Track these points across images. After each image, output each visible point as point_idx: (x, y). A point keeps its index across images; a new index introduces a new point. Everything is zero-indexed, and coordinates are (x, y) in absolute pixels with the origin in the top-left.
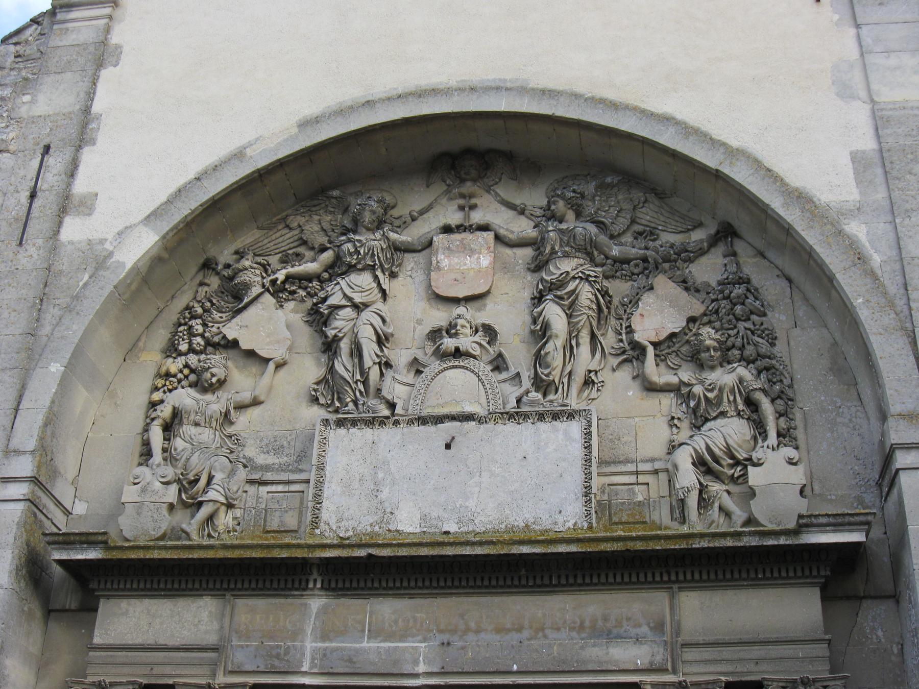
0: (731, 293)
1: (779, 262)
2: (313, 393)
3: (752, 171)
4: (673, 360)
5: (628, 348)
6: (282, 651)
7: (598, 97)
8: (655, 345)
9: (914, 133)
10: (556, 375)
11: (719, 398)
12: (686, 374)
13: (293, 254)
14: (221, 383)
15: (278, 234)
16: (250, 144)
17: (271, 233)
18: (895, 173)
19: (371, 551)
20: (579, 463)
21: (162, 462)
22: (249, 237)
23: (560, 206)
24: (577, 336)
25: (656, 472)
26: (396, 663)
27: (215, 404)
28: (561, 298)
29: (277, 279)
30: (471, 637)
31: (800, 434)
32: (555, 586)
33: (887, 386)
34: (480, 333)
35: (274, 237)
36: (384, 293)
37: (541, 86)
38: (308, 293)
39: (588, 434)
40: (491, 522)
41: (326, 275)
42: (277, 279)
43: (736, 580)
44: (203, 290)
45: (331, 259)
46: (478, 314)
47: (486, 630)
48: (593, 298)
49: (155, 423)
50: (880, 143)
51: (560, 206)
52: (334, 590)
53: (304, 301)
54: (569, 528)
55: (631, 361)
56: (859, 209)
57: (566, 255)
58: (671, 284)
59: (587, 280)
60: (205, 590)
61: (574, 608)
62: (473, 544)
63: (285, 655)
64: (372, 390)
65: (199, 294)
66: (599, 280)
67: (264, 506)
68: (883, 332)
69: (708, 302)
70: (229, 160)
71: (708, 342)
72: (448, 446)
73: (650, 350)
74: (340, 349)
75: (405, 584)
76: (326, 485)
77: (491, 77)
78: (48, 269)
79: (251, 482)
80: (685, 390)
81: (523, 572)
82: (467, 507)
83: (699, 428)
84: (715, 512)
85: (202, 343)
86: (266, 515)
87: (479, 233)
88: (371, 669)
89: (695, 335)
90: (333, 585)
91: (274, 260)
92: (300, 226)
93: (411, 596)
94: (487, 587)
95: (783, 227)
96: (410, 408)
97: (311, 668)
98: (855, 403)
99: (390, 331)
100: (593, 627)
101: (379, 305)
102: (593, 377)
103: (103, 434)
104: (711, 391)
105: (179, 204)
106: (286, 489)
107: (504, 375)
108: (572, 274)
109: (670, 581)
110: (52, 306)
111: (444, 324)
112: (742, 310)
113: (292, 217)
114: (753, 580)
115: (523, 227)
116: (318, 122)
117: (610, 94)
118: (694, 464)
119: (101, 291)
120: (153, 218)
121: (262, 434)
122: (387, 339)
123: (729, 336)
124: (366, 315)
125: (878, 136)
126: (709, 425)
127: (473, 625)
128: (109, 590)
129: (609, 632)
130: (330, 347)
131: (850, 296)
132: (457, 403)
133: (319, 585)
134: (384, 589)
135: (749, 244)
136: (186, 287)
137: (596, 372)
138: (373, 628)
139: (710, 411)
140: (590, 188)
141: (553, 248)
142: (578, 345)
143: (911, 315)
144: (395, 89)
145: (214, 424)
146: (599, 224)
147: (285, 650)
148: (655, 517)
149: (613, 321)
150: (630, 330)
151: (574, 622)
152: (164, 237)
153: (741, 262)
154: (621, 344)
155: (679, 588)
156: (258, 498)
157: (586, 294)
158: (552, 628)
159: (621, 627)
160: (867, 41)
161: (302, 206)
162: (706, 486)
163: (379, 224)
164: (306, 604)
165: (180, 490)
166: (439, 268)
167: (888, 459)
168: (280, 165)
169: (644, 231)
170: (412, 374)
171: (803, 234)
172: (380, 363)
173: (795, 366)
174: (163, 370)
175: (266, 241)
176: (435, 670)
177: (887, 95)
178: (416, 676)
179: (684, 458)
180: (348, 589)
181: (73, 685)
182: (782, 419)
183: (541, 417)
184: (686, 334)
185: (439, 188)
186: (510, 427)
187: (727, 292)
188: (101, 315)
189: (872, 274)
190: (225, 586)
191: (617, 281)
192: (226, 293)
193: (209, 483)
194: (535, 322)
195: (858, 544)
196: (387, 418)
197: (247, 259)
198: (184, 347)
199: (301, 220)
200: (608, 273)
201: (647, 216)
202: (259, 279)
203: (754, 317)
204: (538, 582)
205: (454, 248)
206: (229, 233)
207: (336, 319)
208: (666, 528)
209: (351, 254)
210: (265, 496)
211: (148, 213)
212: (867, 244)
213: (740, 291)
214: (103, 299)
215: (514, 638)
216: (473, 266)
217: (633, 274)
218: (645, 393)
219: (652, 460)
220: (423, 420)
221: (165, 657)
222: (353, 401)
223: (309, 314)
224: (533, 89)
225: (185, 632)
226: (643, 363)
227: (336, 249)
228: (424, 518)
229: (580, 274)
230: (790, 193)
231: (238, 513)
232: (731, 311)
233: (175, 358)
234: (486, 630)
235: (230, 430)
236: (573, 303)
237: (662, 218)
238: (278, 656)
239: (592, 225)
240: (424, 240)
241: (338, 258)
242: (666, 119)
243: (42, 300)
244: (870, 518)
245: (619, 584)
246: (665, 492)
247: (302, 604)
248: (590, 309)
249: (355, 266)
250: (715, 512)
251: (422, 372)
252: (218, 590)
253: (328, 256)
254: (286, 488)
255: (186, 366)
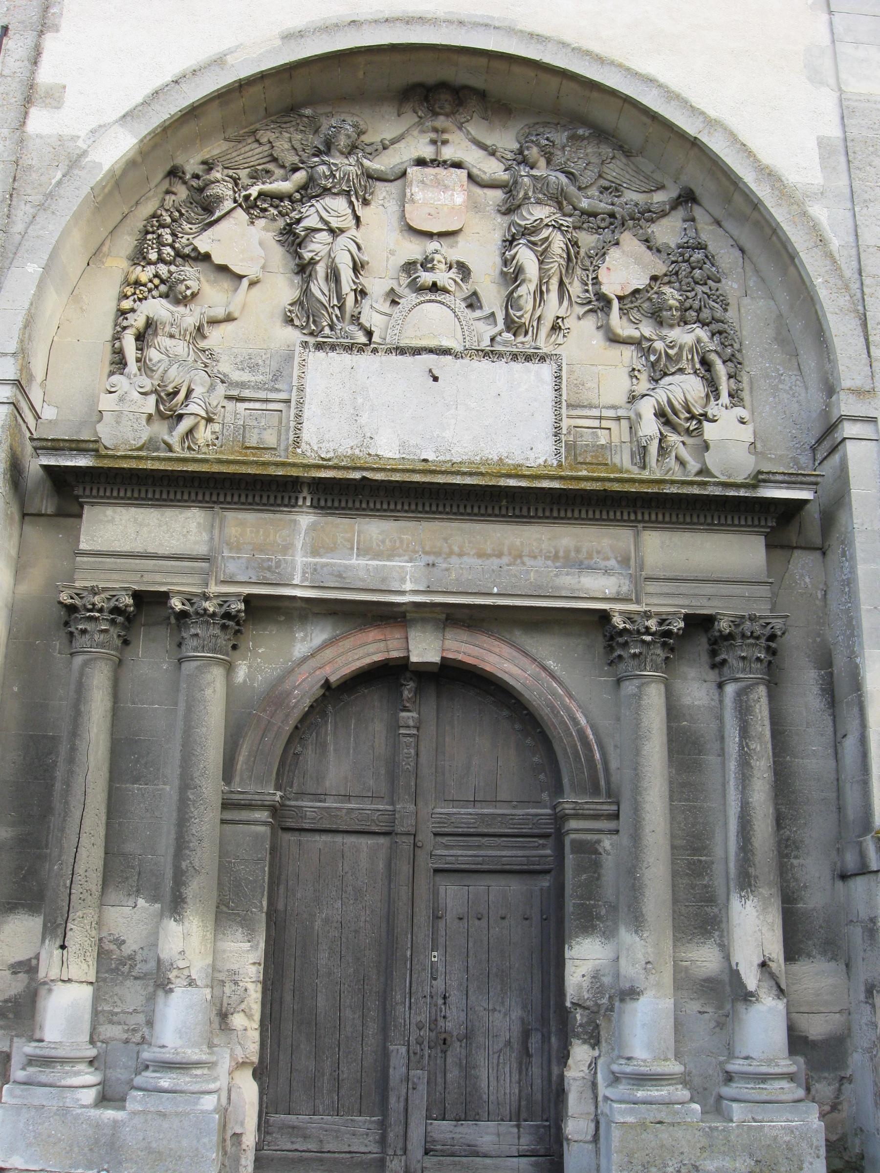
0: (691, 256)
1: (736, 233)
2: (289, 314)
3: (728, 143)
4: (635, 315)
5: (594, 299)
6: (273, 564)
7: (584, 49)
8: (620, 298)
9: (876, 126)
10: (526, 319)
11: (679, 355)
12: (647, 329)
13: (262, 170)
14: (194, 295)
15: (247, 148)
16: (230, 52)
17: (240, 146)
18: (856, 163)
19: (366, 474)
20: (550, 404)
21: (138, 373)
22: (214, 149)
23: (533, 152)
24: (547, 282)
25: (618, 419)
26: (384, 580)
27: (189, 317)
28: (534, 244)
29: (250, 195)
30: (454, 560)
31: (746, 395)
32: (533, 517)
33: (840, 362)
34: (454, 270)
35: (243, 151)
36: (357, 219)
37: (529, 30)
38: (280, 212)
39: (558, 377)
40: (467, 454)
41: (297, 196)
42: (250, 195)
43: (694, 524)
44: (170, 199)
45: (304, 180)
46: (450, 250)
47: (469, 554)
48: (564, 247)
49: (127, 331)
50: (845, 132)
51: (533, 152)
52: (322, 508)
53: (276, 220)
54: (540, 465)
55: (595, 312)
56: (822, 193)
57: (539, 202)
58: (636, 242)
59: (559, 228)
60: (193, 501)
61: (550, 539)
62: (464, 474)
63: (277, 567)
64: (348, 316)
65: (167, 202)
66: (570, 230)
67: (242, 423)
68: (838, 312)
69: (668, 262)
70: (209, 65)
71: (672, 302)
72: (436, 379)
73: (616, 304)
74: (316, 272)
75: (392, 506)
76: (306, 406)
77: (479, 13)
78: (17, 163)
79: (229, 398)
80: (645, 345)
81: (504, 503)
82: (444, 438)
83: (656, 381)
84: (671, 461)
85: (172, 253)
86: (244, 431)
87: (453, 170)
88: (360, 585)
89: (656, 293)
90: (322, 503)
91: (243, 174)
92: (270, 142)
93: (397, 519)
94: (469, 514)
95: (752, 201)
96: (388, 337)
97: (302, 581)
98: (795, 373)
99: (366, 259)
100: (567, 557)
101: (353, 232)
102: (561, 324)
103: (69, 339)
104: (671, 348)
105: (157, 107)
106: (264, 408)
107: (478, 313)
108: (546, 221)
109: (636, 521)
110: (23, 202)
111: (420, 257)
112: (701, 275)
113: (262, 132)
114: (708, 525)
115: (493, 169)
116: (302, 36)
117: (596, 48)
118: (655, 415)
119: (77, 192)
120: (129, 118)
121: (236, 350)
122: (362, 267)
123: (688, 298)
124: (342, 240)
125: (844, 125)
126: (667, 380)
127: (456, 549)
128: (95, 497)
129: (581, 563)
130: (304, 269)
131: (811, 274)
132: (435, 336)
133: (308, 503)
134: (372, 510)
135: (707, 211)
136: (151, 193)
137: (563, 319)
138: (361, 546)
139: (669, 367)
140: (560, 137)
141: (526, 194)
142: (548, 290)
143: (864, 300)
144: (381, 11)
145: (188, 338)
146: (569, 175)
147: (276, 563)
148: (617, 460)
149: (579, 271)
150: (596, 281)
151: (550, 552)
152: (142, 141)
153: (699, 228)
154: (587, 295)
155: (644, 527)
156: (236, 414)
157: (558, 243)
158: (529, 556)
159: (592, 558)
160: (839, 29)
161: (273, 122)
162: (666, 437)
163: (352, 149)
164: (295, 521)
165: (157, 401)
166: (413, 201)
167: (831, 428)
168: (262, 77)
169: (610, 187)
170: (388, 303)
171: (772, 210)
172: (355, 290)
173: (744, 333)
174: (132, 278)
175: (234, 154)
176: (421, 589)
177: (855, 86)
178: (402, 593)
179: (647, 408)
180: (336, 509)
181: (63, 589)
182: (732, 380)
183: (515, 357)
184: (648, 292)
185: (410, 118)
186: (485, 364)
187: (687, 255)
188: (77, 216)
189: (830, 255)
190: (214, 498)
191: (584, 232)
192: (195, 204)
193: (187, 396)
194: (506, 263)
195: (805, 502)
196: (366, 345)
197: (218, 171)
198: (153, 256)
199: (272, 136)
200: (576, 224)
201: (615, 170)
202: (231, 193)
203: (710, 282)
204: (517, 512)
205: (428, 182)
206: (198, 141)
207: (312, 241)
208: (627, 471)
209: (326, 177)
210: (243, 412)
211: (123, 113)
212: (828, 228)
213: (699, 256)
214: (80, 200)
215: (496, 561)
216: (447, 202)
217: (599, 228)
218: (608, 343)
219: (614, 407)
220: (401, 351)
221: (155, 565)
222: (329, 325)
223: (281, 233)
224: (521, 31)
225: (174, 542)
226: (608, 315)
227: (310, 170)
228: (403, 445)
229: (553, 223)
230: (762, 169)
231: (217, 427)
232: (689, 275)
233: (144, 267)
234: (469, 554)
235: (203, 344)
236: (546, 250)
237: (628, 177)
238: (269, 569)
239: (563, 175)
240: (398, 171)
241: (311, 179)
242: (649, 81)
243: (11, 195)
244: (819, 479)
245: (590, 520)
246: (626, 437)
247: (291, 521)
248: (561, 257)
249: (329, 189)
250: (671, 461)
251: (399, 303)
252: (207, 502)
253: (300, 176)
254: (264, 406)
255: (156, 276)
